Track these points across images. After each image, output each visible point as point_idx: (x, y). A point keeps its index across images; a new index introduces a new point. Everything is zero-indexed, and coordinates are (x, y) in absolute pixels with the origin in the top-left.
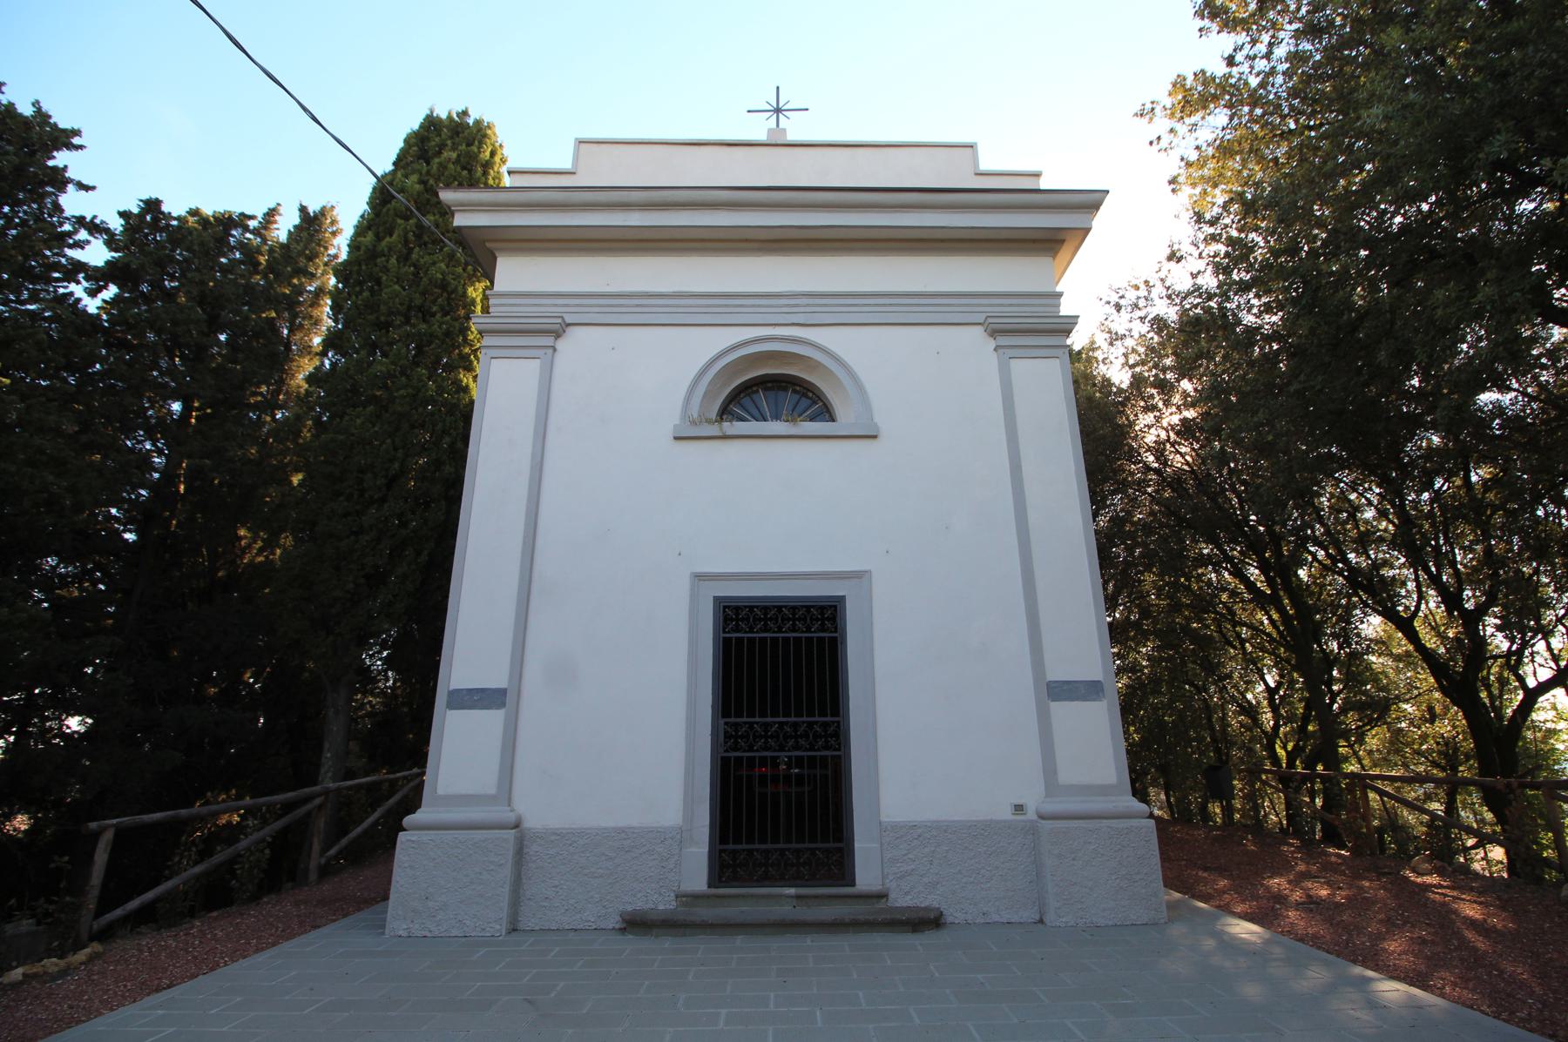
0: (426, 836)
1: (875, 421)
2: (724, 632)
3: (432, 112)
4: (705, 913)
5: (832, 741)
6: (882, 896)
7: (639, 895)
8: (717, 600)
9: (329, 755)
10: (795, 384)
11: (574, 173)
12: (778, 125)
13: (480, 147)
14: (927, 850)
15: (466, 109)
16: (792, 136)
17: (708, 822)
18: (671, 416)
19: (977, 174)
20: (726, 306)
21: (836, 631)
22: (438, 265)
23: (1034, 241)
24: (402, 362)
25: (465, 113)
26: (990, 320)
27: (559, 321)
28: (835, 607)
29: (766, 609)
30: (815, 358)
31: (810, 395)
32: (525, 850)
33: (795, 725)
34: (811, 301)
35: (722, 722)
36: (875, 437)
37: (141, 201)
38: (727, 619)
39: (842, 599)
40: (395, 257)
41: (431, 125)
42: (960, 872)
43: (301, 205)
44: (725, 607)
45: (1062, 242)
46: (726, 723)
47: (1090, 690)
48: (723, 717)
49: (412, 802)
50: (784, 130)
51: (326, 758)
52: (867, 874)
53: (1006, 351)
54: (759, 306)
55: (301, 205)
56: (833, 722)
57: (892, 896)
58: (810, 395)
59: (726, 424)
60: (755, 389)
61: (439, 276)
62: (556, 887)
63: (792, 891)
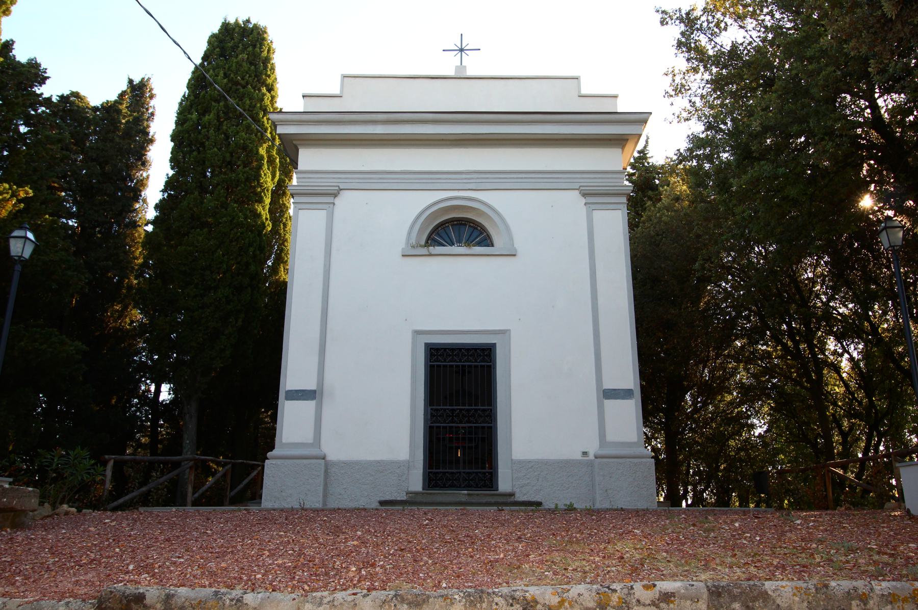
0: (279, 462)
1: (515, 246)
2: (430, 362)
3: (225, 21)
4: (419, 499)
5: (487, 419)
6: (512, 495)
7: (387, 493)
8: (427, 345)
9: (188, 442)
10: (470, 222)
12: (461, 64)
13: (261, 48)
14: (536, 473)
15: (249, 18)
16: (470, 73)
17: (422, 458)
19: (579, 96)
20: (431, 179)
21: (490, 362)
22: (240, 134)
23: (610, 140)
24: (221, 200)
26: (582, 188)
27: (337, 188)
28: (491, 349)
29: (453, 350)
30: (482, 209)
31: (479, 228)
32: (329, 471)
35: (429, 409)
36: (515, 255)
37: (58, 96)
38: (432, 355)
39: (494, 345)
40: (213, 128)
41: (227, 29)
42: (552, 485)
43: (129, 79)
44: (431, 349)
45: (628, 140)
46: (432, 409)
47: (626, 394)
48: (430, 406)
50: (465, 67)
51: (186, 443)
52: (504, 484)
53: (590, 205)
54: (450, 179)
55: (129, 79)
56: (488, 409)
57: (517, 495)
58: (479, 228)
59: (431, 248)
60: (447, 225)
61: (242, 141)
62: (345, 489)
63: (466, 492)
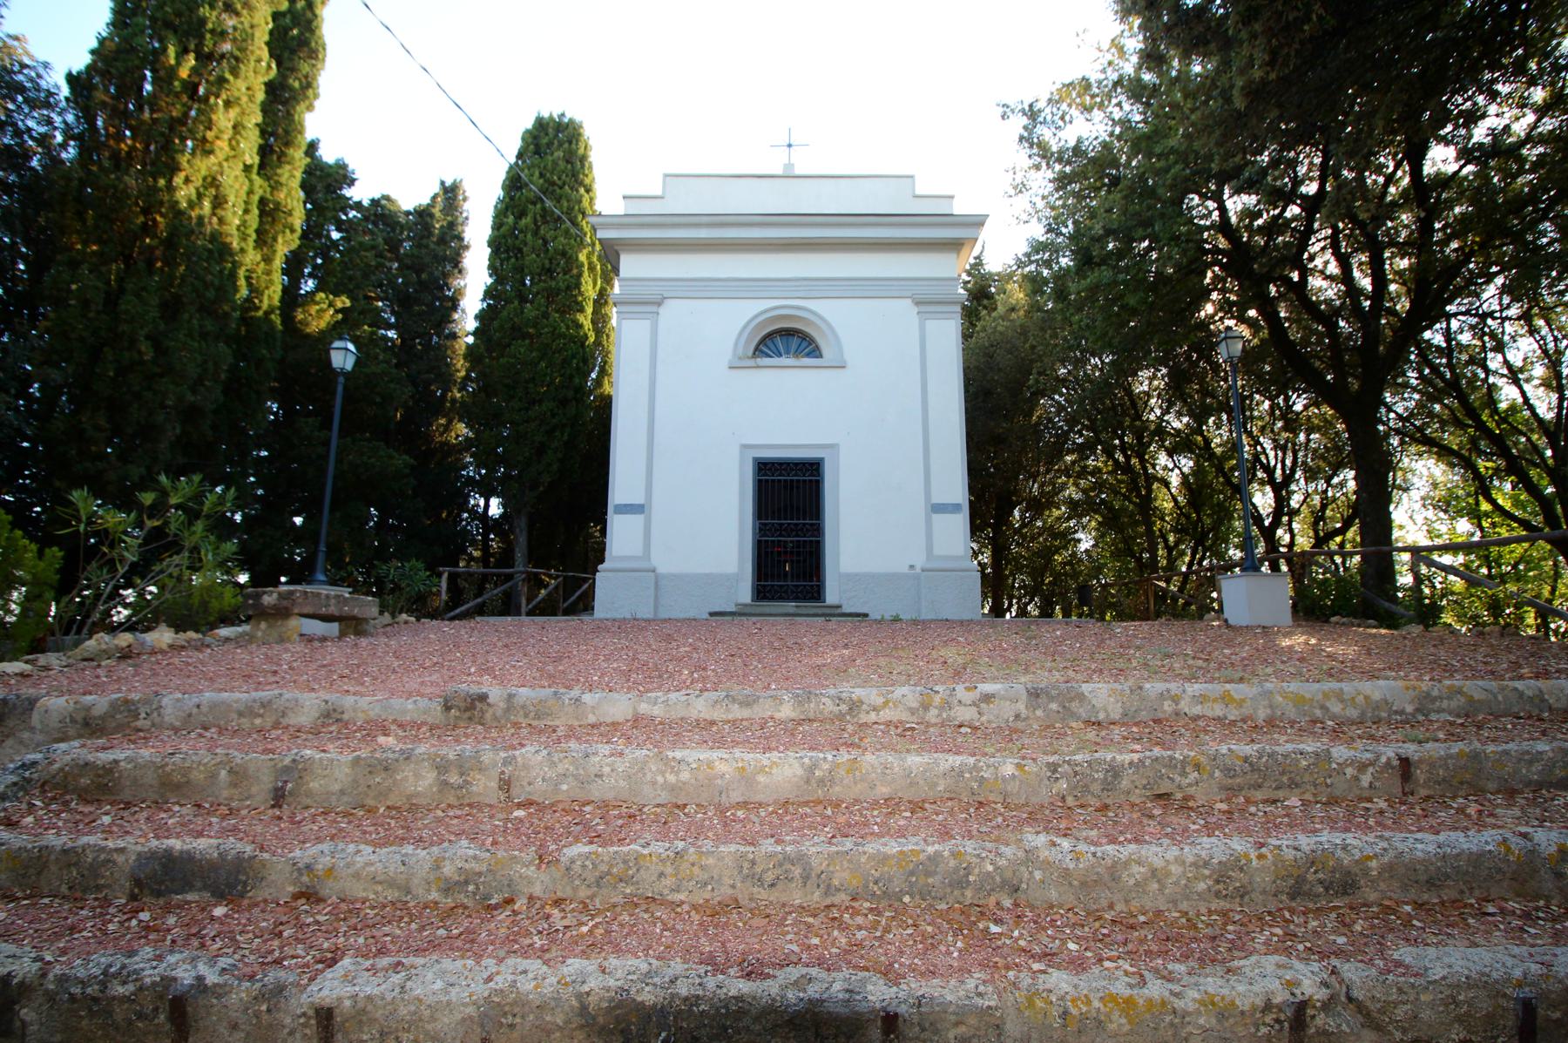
0: (610, 574)
11: (662, 198)
18: (727, 355)
23: (945, 244)
25: (563, 115)
33: (796, 525)
34: (805, 283)
38: (760, 469)
39: (822, 459)
45: (962, 244)
47: (956, 508)
49: (602, 561)
52: (832, 595)
